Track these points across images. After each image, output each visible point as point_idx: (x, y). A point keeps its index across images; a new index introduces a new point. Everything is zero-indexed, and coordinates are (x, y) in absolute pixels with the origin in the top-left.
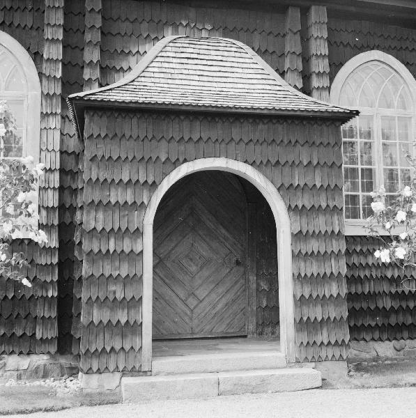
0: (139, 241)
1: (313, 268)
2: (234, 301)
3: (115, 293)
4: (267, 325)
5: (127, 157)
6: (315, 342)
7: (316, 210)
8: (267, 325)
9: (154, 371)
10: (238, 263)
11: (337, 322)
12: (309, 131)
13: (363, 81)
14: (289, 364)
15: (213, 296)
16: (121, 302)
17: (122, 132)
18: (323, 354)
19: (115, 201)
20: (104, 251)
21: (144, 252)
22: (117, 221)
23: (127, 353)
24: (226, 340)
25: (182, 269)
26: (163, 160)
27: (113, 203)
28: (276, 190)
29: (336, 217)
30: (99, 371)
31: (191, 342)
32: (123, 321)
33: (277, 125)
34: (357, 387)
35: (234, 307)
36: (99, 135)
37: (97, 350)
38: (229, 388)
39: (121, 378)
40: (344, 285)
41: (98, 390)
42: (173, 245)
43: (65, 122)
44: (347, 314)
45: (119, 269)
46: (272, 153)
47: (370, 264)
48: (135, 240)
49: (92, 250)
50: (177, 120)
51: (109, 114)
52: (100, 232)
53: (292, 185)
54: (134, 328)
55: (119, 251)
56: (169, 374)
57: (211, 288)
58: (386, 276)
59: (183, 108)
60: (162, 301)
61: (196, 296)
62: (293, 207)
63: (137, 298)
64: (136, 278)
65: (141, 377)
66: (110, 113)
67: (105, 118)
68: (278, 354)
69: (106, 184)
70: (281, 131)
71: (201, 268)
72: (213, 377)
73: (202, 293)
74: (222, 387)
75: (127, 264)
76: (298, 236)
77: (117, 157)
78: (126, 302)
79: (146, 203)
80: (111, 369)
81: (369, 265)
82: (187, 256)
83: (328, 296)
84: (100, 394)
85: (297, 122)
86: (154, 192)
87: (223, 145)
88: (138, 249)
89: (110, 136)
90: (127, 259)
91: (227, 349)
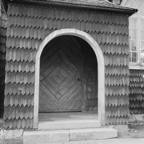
0: (33, 66)
1: (114, 82)
2: (76, 96)
3: (21, 91)
4: (91, 106)
5: (28, 26)
6: (114, 116)
7: (116, 55)
8: (91, 106)
9: (39, 129)
10: (78, 80)
11: (124, 107)
12: (114, 19)
13: (134, 3)
14: (102, 126)
15: (68, 93)
16: (24, 96)
17: (26, 15)
18: (118, 122)
19: (22, 47)
20: (16, 71)
21: (35, 72)
22: (23, 57)
23: (26, 120)
24: (73, 113)
25: (54, 82)
26: (46, 28)
27: (21, 48)
28: (98, 45)
29: (125, 59)
30: (12, 129)
31: (57, 113)
32: (25, 105)
33: (99, 15)
34: (133, 137)
35: (77, 99)
36: (15, 15)
37: (11, 118)
38: (74, 137)
39: (23, 132)
40: (128, 90)
41: (12, 138)
42: (51, 71)
43: (3, 14)
44: (129, 103)
45: (23, 80)
46: (97, 28)
47: (134, 82)
48: (31, 66)
49: (10, 70)
50: (53, 10)
51: (20, 5)
52: (14, 62)
53: (106, 43)
54: (30, 108)
55: (23, 71)
56: (46, 130)
57: (67, 90)
58: (140, 87)
59: (56, 3)
60: (45, 95)
61: (60, 93)
62: (106, 53)
63: (31, 94)
64: (31, 84)
65: (33, 131)
66: (20, 4)
67: (18, 7)
68: (97, 121)
69: (18, 38)
70: (102, 18)
71: (63, 81)
72: (66, 132)
73: (62, 92)
74: (71, 137)
75: (27, 78)
76: (107, 67)
77: (23, 26)
78: (121, 76)
79: (37, 48)
80: (19, 127)
81: (134, 82)
82: (57, 76)
83: (120, 95)
84: (13, 139)
85: (109, 14)
86: (41, 43)
87: (74, 23)
88: (32, 71)
89: (20, 15)
90: (27, 75)
91: (74, 118)
